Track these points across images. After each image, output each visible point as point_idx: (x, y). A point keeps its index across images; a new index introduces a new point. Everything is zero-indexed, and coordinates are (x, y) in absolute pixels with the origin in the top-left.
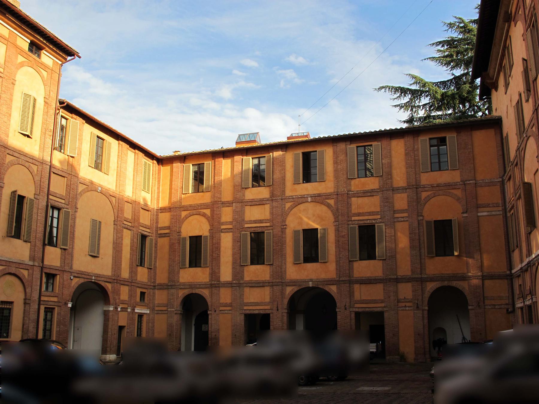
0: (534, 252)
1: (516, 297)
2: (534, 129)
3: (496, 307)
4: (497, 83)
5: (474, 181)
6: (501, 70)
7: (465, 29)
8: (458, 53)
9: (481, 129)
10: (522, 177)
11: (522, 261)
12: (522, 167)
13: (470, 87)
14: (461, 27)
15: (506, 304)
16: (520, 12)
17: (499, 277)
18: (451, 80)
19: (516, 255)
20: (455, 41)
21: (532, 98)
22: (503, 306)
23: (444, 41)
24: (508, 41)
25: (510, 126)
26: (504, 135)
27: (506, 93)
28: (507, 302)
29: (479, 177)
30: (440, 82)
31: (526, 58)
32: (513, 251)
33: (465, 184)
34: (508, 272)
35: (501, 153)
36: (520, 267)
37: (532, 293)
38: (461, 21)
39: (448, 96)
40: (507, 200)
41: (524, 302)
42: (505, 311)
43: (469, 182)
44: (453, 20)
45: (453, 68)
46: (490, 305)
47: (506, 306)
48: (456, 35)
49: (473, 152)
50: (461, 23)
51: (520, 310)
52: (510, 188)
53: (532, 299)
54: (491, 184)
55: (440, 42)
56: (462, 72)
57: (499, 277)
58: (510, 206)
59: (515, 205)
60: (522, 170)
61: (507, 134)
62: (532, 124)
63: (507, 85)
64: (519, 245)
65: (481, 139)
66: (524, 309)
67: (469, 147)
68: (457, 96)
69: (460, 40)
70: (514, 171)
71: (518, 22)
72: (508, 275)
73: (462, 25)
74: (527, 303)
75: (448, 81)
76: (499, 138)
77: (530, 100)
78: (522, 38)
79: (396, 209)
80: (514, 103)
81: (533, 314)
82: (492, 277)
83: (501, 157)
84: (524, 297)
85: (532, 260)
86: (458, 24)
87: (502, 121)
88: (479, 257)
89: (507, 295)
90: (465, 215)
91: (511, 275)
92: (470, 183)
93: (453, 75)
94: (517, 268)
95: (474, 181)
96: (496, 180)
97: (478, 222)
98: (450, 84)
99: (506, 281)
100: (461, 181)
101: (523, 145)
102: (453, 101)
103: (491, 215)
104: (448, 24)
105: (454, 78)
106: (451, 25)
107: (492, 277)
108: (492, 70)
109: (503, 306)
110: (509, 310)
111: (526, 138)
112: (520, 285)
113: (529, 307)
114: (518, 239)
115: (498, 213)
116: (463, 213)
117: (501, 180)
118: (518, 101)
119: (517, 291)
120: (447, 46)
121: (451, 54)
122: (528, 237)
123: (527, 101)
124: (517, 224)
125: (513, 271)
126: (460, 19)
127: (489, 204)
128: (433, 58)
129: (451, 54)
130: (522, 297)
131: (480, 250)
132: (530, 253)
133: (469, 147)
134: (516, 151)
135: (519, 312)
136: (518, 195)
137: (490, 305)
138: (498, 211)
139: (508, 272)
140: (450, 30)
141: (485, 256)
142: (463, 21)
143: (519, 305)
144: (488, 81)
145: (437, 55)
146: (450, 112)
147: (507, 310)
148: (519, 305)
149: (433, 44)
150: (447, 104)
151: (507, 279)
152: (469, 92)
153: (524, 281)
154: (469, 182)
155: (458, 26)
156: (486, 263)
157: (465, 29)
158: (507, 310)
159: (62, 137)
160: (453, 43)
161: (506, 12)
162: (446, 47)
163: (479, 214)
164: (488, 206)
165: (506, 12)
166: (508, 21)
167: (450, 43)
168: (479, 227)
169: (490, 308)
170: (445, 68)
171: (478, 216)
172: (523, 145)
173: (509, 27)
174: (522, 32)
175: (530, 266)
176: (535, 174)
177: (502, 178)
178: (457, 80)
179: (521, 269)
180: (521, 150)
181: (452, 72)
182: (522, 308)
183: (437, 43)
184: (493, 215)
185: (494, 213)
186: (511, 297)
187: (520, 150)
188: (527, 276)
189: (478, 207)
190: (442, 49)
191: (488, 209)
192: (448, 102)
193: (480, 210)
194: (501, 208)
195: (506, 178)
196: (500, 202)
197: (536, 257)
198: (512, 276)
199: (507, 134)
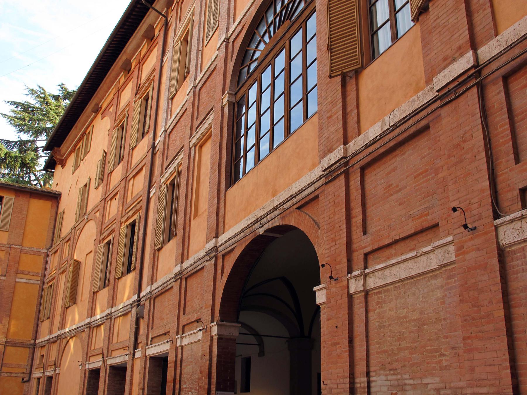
0: (68, 326)
1: (35, 366)
2: (98, 213)
3: (13, 375)
4: (66, 161)
5: (20, 247)
6: (74, 151)
7: (44, 101)
8: (31, 119)
9: (40, 199)
10: (72, 255)
11: (50, 333)
12: (74, 245)
13: (35, 155)
14: (41, 97)
15: (24, 373)
16: (111, 110)
17: (23, 345)
18: (16, 142)
19: (45, 326)
20: (31, 107)
21: (103, 187)
22: (19, 375)
23: (20, 103)
24: (90, 129)
25: (69, 204)
26: (60, 210)
27: (73, 174)
28: (25, 371)
29: (26, 244)
30: (5, 140)
31: (106, 151)
32: (42, 321)
33: (10, 248)
34: (32, 341)
35: (52, 226)
36: (47, 338)
37: (56, 365)
38: (43, 92)
39: (11, 157)
40: (48, 271)
41: (44, 373)
42: (21, 379)
43: (14, 246)
44: (36, 88)
45: (22, 130)
46: (7, 373)
47: (22, 375)
48: (33, 102)
49: (26, 218)
50: (42, 94)
51: (36, 380)
52: (54, 261)
53: (55, 370)
54: (36, 253)
55: (15, 103)
56: (29, 139)
57: (23, 345)
58: (50, 278)
59: (57, 278)
60: (73, 248)
61: (64, 210)
62: (96, 210)
63: (76, 167)
64: (51, 317)
65: (38, 207)
66: (41, 379)
67: (24, 212)
68: (19, 160)
69: (38, 109)
70: (63, 246)
71: (106, 118)
72: (31, 345)
73: (42, 96)
74: (48, 374)
75: (13, 142)
76: (54, 211)
77: (100, 188)
78: (107, 133)
79: (21, 268)
80: (81, 185)
81: (53, 385)
82: (14, 344)
83: (52, 230)
84: (44, 368)
85: (64, 333)
86: (39, 93)
87: (61, 197)
88: (7, 323)
89: (26, 364)
90: (3, 278)
91: (35, 345)
92: (16, 248)
93: (19, 137)
94: (43, 338)
95: (20, 247)
96: (42, 251)
97: (14, 288)
98: (14, 145)
99: (28, 350)
100: (7, 244)
101: (81, 226)
102: (15, 163)
103: (28, 283)
104: (30, 90)
105: (19, 141)
106: (32, 92)
107: (14, 344)
108: (65, 147)
109: (19, 375)
110: (25, 379)
111: (86, 221)
112: (43, 356)
113: (50, 378)
114: (52, 311)
115: (36, 282)
116: (1, 276)
117: (46, 251)
118: (86, 185)
119: (37, 361)
120: (21, 108)
121: (24, 118)
122: (64, 311)
123: (97, 188)
124: (54, 296)
125: (37, 341)
126: (43, 89)
127: (29, 272)
128: (5, 116)
129: (24, 118)
130: (44, 367)
131: (10, 316)
132: (63, 325)
133: (24, 212)
134: (72, 229)
135: (34, 383)
136: (62, 270)
137: (7, 373)
138: (37, 281)
139: (32, 341)
140: (30, 95)
141: (13, 322)
142: (44, 93)
143: (37, 374)
144: (58, 157)
145: (10, 114)
146: (6, 171)
147: (23, 379)
148: (37, 374)
149: (8, 102)
150: (8, 165)
151: (30, 348)
152: (32, 160)
153: (48, 351)
154: (14, 246)
155: (39, 95)
156: (12, 329)
157: (44, 101)
158: (23, 379)
159: (444, 266)
160: (28, 108)
161: (97, 105)
162: (19, 109)
163: (17, 280)
164: (28, 273)
165: (97, 105)
166: (95, 112)
167: (26, 108)
168: (14, 293)
169: (6, 375)
170: (14, 128)
171: (16, 282)
172: (81, 226)
173: (95, 117)
174: (109, 128)
175: (61, 339)
176: (87, 255)
177: (48, 249)
178: (21, 144)
179: (48, 340)
180: (78, 229)
181: (19, 134)
182: (39, 379)
183: (12, 102)
184: (31, 283)
185: (32, 282)
186: (29, 366)
187: (77, 228)
188: (54, 348)
189: (18, 272)
190: (16, 109)
191: (27, 277)
192: (9, 163)
193: (19, 275)
194: (39, 278)
195: (52, 251)
196: (41, 272)
197: (70, 331)
198: (35, 345)
199: (64, 210)
